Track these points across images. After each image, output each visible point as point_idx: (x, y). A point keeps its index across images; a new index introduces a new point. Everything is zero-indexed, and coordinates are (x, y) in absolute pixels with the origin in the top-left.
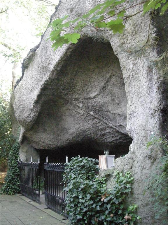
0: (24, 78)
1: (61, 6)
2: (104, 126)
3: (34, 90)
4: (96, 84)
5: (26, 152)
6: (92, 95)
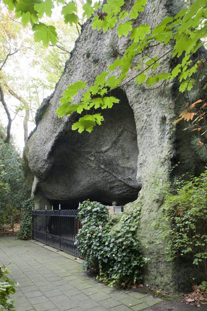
0: (38, 129)
1: (77, 51)
2: (113, 179)
3: (48, 141)
4: (108, 138)
5: (40, 202)
6: (104, 149)
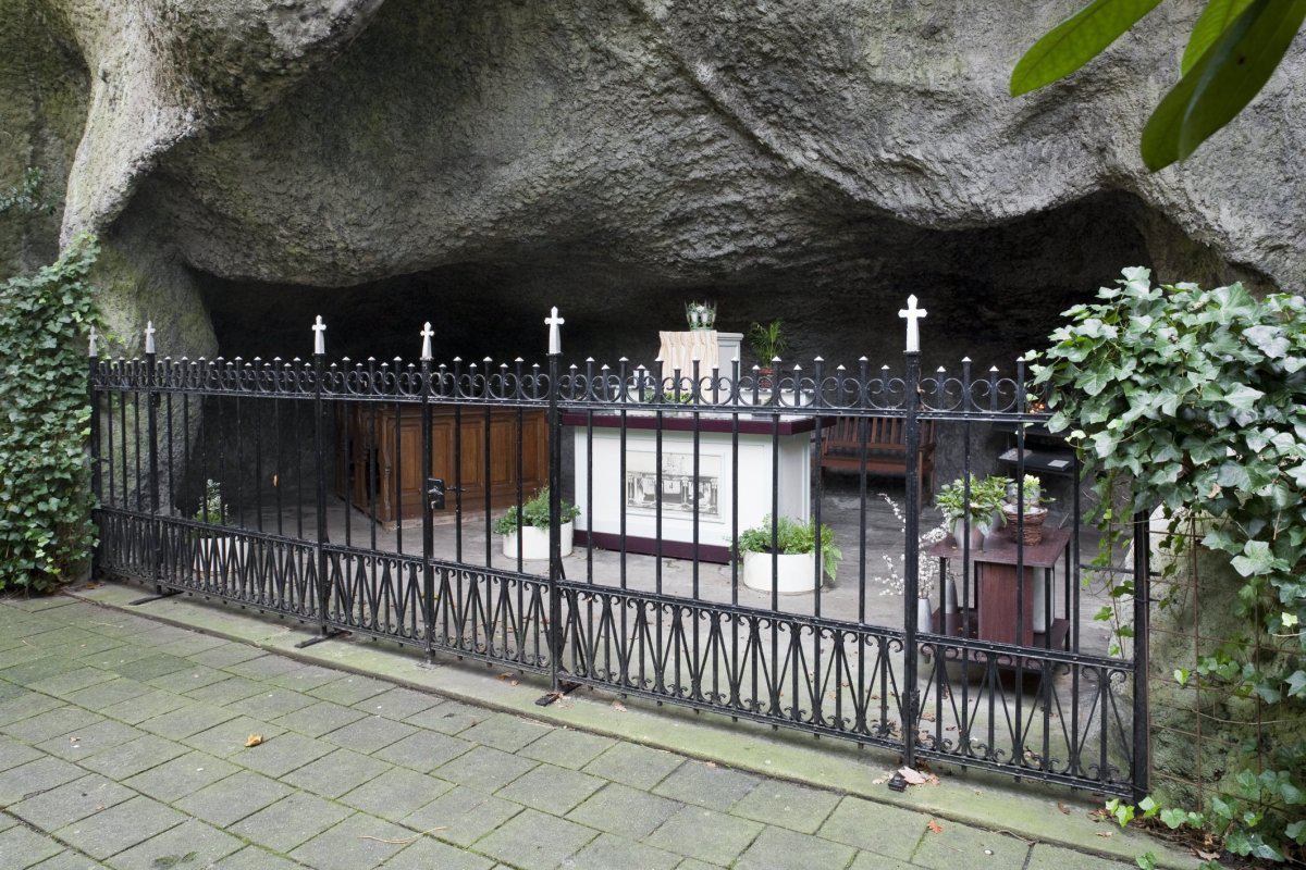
2: (731, 166)
